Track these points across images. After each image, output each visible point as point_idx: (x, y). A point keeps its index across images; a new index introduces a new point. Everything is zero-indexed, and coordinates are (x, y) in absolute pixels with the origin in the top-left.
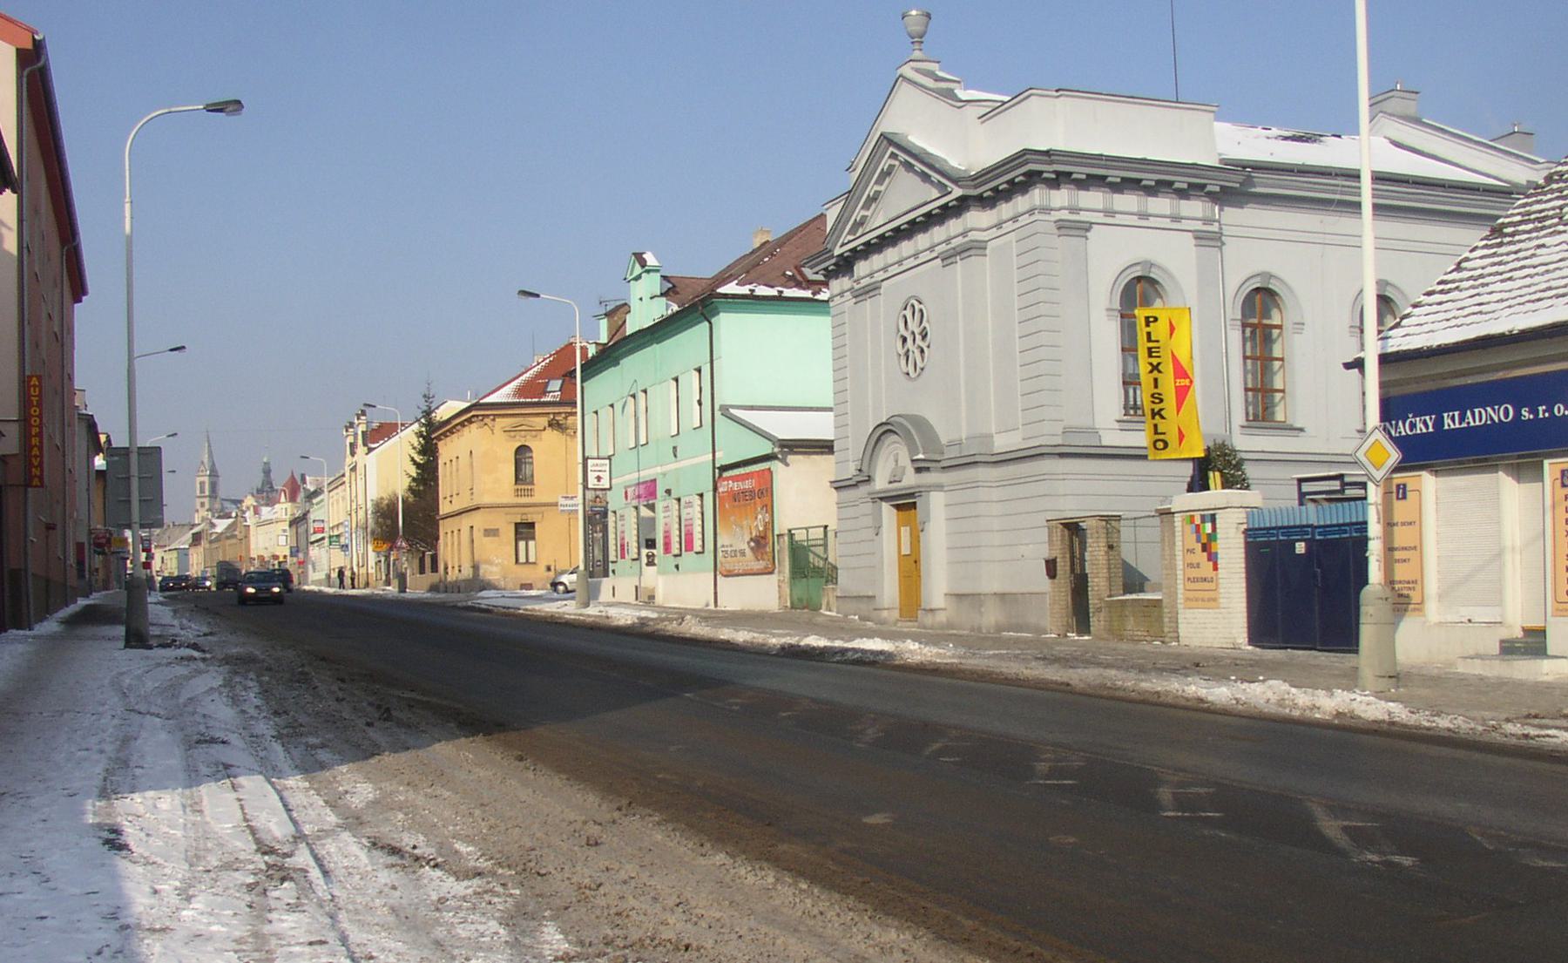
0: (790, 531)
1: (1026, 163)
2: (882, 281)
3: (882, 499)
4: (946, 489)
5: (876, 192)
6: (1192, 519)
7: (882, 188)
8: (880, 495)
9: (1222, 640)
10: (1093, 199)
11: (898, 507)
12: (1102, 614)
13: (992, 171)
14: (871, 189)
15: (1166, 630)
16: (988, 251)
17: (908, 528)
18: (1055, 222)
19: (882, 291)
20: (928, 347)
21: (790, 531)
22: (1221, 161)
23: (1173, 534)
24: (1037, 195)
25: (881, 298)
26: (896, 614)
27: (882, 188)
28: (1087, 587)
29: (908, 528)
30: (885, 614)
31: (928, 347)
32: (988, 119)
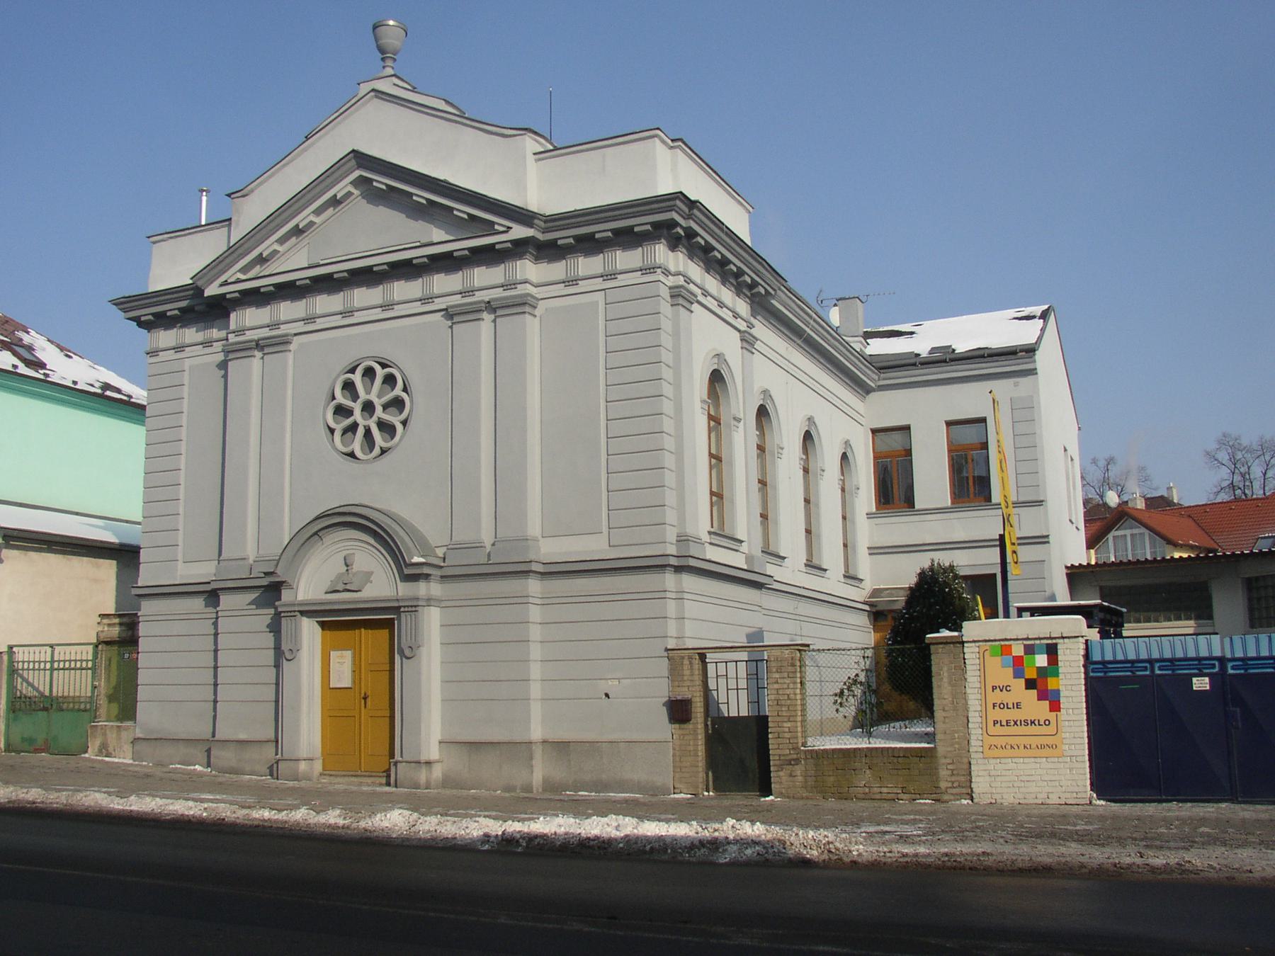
0: (11, 647)
1: (670, 209)
2: (296, 335)
3: (303, 613)
4: (443, 604)
5: (311, 221)
6: (1006, 650)
7: (317, 220)
8: (301, 609)
9: (1068, 795)
10: (287, 310)
11: (323, 625)
12: (798, 770)
13: (555, 220)
14: (301, 220)
15: (943, 785)
16: (537, 312)
17: (348, 654)
18: (670, 288)
19: (292, 347)
20: (404, 423)
21: (11, 647)
22: (668, 276)
23: (963, 670)
24: (661, 252)
25: (290, 356)
26: (318, 766)
27: (317, 220)
28: (767, 733)
29: (348, 654)
30: (303, 766)
31: (404, 423)
32: (550, 158)
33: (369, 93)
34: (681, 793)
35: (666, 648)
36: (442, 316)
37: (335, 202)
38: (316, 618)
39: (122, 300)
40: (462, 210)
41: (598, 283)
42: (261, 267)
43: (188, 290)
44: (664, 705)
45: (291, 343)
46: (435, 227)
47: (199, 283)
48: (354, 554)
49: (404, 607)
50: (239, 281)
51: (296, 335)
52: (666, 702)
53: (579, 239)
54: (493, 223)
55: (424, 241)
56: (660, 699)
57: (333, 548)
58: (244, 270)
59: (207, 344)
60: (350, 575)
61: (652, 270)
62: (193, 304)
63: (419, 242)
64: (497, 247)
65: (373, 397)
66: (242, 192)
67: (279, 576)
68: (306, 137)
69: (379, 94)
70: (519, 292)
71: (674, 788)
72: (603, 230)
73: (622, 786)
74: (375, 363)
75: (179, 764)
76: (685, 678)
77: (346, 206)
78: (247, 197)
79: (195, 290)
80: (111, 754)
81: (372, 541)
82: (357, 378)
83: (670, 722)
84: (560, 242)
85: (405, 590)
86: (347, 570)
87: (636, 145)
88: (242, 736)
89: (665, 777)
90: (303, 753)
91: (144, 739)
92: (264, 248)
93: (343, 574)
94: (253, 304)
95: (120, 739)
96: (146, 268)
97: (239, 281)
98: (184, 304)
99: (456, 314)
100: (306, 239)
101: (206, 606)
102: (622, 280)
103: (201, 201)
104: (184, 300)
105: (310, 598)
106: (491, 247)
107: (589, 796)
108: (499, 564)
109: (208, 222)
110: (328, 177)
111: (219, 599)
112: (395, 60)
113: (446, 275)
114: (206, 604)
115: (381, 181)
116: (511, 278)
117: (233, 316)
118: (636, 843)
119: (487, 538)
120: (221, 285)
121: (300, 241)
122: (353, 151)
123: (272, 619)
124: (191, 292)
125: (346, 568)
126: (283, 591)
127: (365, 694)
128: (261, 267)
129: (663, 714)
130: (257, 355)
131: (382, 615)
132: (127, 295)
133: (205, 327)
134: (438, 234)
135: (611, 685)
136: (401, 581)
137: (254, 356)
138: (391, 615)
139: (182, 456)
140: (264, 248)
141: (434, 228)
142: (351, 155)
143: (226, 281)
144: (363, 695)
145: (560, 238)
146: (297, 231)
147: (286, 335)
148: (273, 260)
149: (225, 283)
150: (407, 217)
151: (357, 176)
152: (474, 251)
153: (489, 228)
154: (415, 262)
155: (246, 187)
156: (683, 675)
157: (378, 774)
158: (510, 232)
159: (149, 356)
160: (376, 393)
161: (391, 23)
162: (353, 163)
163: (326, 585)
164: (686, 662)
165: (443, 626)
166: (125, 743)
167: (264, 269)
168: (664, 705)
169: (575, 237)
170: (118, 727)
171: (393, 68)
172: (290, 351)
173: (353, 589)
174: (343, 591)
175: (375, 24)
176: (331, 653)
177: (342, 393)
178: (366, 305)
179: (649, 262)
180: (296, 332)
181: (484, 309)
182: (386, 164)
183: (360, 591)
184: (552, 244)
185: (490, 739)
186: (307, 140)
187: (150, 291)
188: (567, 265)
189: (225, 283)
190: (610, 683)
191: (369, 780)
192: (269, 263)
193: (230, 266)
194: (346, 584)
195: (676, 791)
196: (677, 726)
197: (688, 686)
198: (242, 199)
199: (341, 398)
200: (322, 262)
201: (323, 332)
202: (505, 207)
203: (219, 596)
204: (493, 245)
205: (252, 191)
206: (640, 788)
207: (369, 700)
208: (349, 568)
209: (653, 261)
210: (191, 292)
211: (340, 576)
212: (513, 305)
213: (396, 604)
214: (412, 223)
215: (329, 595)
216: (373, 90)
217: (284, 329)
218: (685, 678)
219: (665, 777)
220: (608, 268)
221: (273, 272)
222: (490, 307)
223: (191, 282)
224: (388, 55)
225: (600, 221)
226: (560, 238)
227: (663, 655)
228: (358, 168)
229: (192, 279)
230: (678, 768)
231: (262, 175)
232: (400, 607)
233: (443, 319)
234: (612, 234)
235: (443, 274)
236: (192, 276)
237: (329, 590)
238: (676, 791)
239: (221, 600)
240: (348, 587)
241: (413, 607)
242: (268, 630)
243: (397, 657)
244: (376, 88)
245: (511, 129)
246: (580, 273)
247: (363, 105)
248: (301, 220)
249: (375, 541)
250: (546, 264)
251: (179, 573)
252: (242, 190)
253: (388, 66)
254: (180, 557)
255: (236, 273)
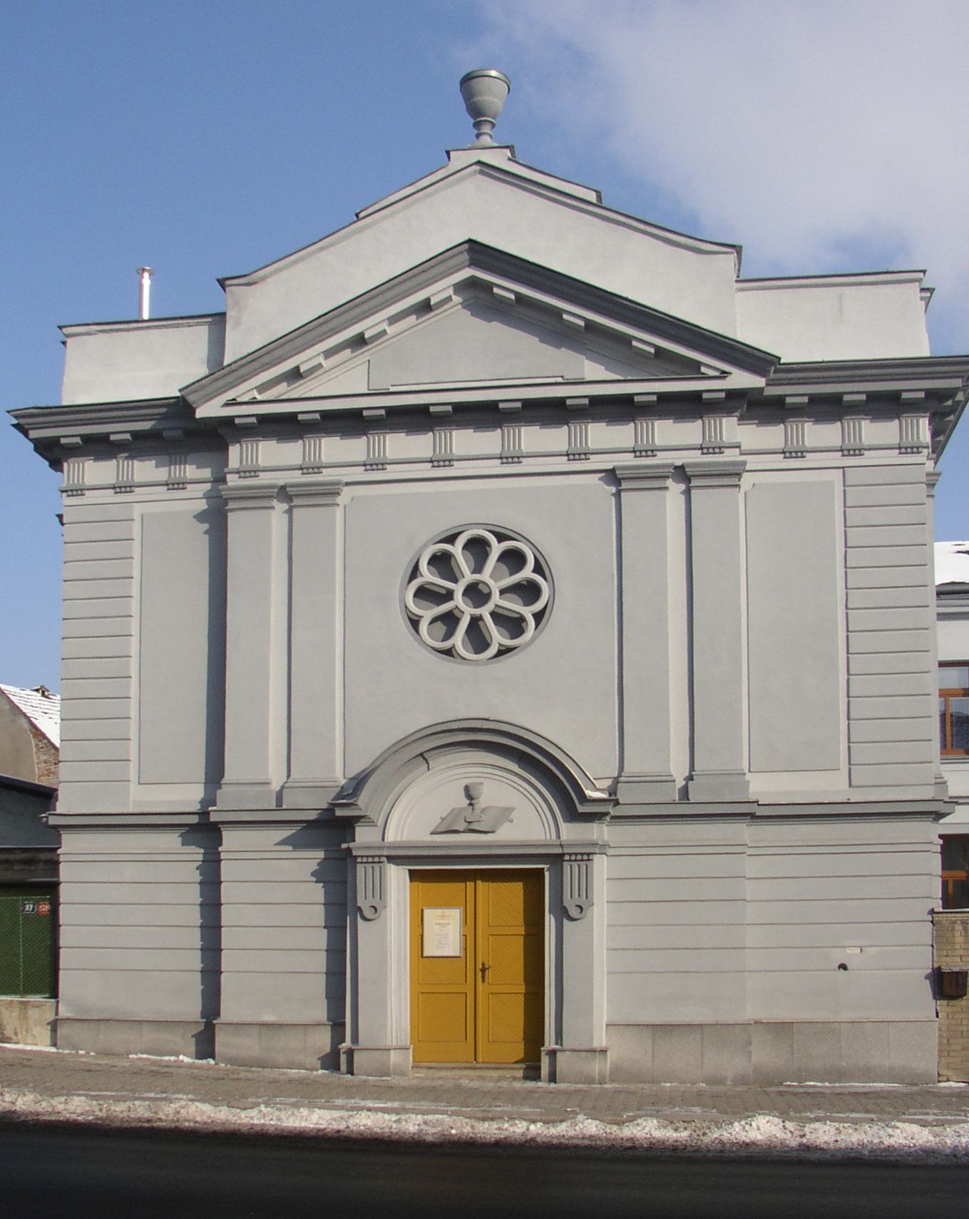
2: (347, 484)
3: (391, 859)
10: (333, 448)
11: (414, 876)
14: (367, 326)
19: (339, 500)
25: (339, 512)
30: (394, 1057)
33: (471, 165)
34: (948, 1080)
35: (933, 909)
36: (600, 479)
37: (425, 307)
38: (410, 865)
39: (32, 411)
40: (646, 340)
41: (836, 459)
42: (288, 386)
43: (161, 406)
44: (926, 977)
45: (338, 494)
46: (587, 359)
47: (191, 399)
48: (482, 783)
49: (362, 857)
50: (254, 402)
51: (347, 484)
52: (929, 974)
53: (87, 439)
54: (698, 364)
55: (570, 375)
56: (920, 971)
57: (445, 775)
58: (262, 388)
59: (173, 485)
60: (477, 811)
61: (181, 486)
62: (160, 427)
63: (562, 377)
64: (300, 417)
65: (485, 576)
66: (248, 278)
67: (360, 809)
68: (357, 215)
69: (486, 169)
70: (726, 459)
71: (939, 1074)
72: (854, 391)
73: (868, 1073)
74: (488, 533)
75: (143, 1053)
76: (957, 946)
77: (431, 318)
78: (253, 286)
79: (180, 408)
80: (11, 1039)
81: (514, 767)
82: (457, 550)
83: (935, 998)
84: (112, 438)
85: (571, 832)
86: (471, 804)
87: (887, 289)
88: (269, 1018)
89: (926, 1061)
90: (392, 1040)
91: (76, 1020)
92: (303, 360)
93: (462, 809)
94: (470, 425)
95: (26, 1018)
96: (57, 371)
97: (254, 402)
98: (146, 425)
99: (231, 499)
100: (365, 354)
101: (183, 845)
102: (870, 458)
103: (141, 286)
104: (147, 420)
105: (404, 838)
106: (696, 396)
107: (864, 1087)
108: (814, 804)
109: (153, 317)
110: (424, 272)
111: (221, 835)
112: (493, 125)
113: (674, 422)
114: (183, 840)
115: (506, 288)
116: (713, 439)
117: (234, 451)
118: (668, 1141)
119: (679, 771)
120: (227, 405)
121: (355, 357)
122: (470, 241)
123: (318, 864)
124: (164, 410)
125: (468, 802)
126: (357, 828)
127: (483, 964)
128: (288, 386)
129: (926, 988)
130: (276, 507)
131: (524, 864)
132: (43, 405)
133: (171, 461)
134: (592, 369)
135: (850, 955)
136: (564, 821)
137: (273, 508)
138: (541, 864)
139: (133, 638)
140: (303, 360)
141: (587, 362)
142: (466, 246)
143: (234, 400)
144: (480, 966)
145: (64, 436)
146: (359, 341)
147: (338, 483)
148: (309, 378)
149: (233, 403)
150: (541, 341)
151: (467, 276)
152: (664, 397)
153: (693, 369)
154: (569, 402)
155: (254, 272)
156: (954, 943)
157: (506, 1066)
158: (728, 378)
159: (64, 494)
160: (493, 577)
161: (493, 73)
162: (466, 257)
163: (434, 822)
164: (959, 927)
165: (610, 879)
166: (36, 1025)
167: (291, 390)
168: (926, 978)
169: (83, 437)
170: (22, 1002)
171: (491, 137)
172: (338, 505)
173: (483, 829)
174: (464, 832)
175: (469, 74)
176: (426, 912)
177: (428, 568)
178: (686, 443)
179: (76, 482)
180: (349, 480)
181: (275, 495)
182: (528, 265)
183: (493, 832)
184: (779, 402)
185: (687, 1020)
186: (357, 221)
187: (65, 403)
188: (118, 466)
189: (233, 403)
190: (848, 951)
191: (495, 1074)
192: (302, 382)
193: (244, 379)
194: (470, 822)
195: (941, 1079)
196: (944, 1002)
197: (961, 956)
198: (245, 287)
199: (428, 576)
200: (392, 389)
201: (428, 483)
202: (728, 344)
203: (60, 835)
204: (295, 414)
205: (263, 279)
206: (891, 1076)
207: (489, 973)
208: (473, 802)
209: (130, 478)
210: (164, 410)
211: (455, 813)
212: (720, 475)
213: (558, 851)
214: (549, 350)
215: (436, 836)
216: (479, 163)
217: (327, 475)
218: (957, 946)
219: (926, 1061)
220: (175, 474)
221: (303, 396)
222: (284, 493)
223: (178, 394)
224: (488, 119)
225: (782, 382)
226: (64, 436)
227: (926, 919)
228: (469, 266)
229: (180, 391)
230: (944, 1051)
231: (291, 255)
232: (563, 855)
233: (602, 482)
234: (82, 440)
235: (472, 430)
236: (180, 387)
237: (438, 830)
238: (941, 1079)
239: (224, 837)
240: (474, 826)
241: (585, 856)
242: (314, 879)
243: (550, 922)
244: (483, 159)
245: (711, 243)
246: (187, 474)
247: (459, 181)
248: (367, 326)
249: (520, 767)
250: (755, 426)
251: (132, 798)
252: (245, 276)
253: (484, 133)
254: (133, 776)
255: (252, 389)
